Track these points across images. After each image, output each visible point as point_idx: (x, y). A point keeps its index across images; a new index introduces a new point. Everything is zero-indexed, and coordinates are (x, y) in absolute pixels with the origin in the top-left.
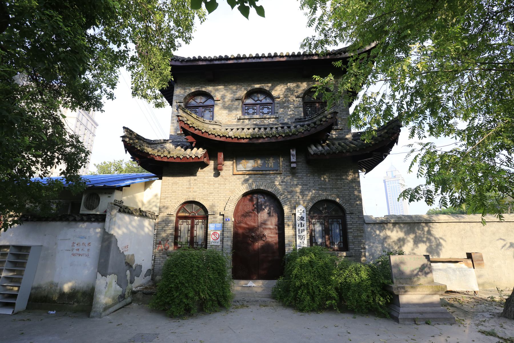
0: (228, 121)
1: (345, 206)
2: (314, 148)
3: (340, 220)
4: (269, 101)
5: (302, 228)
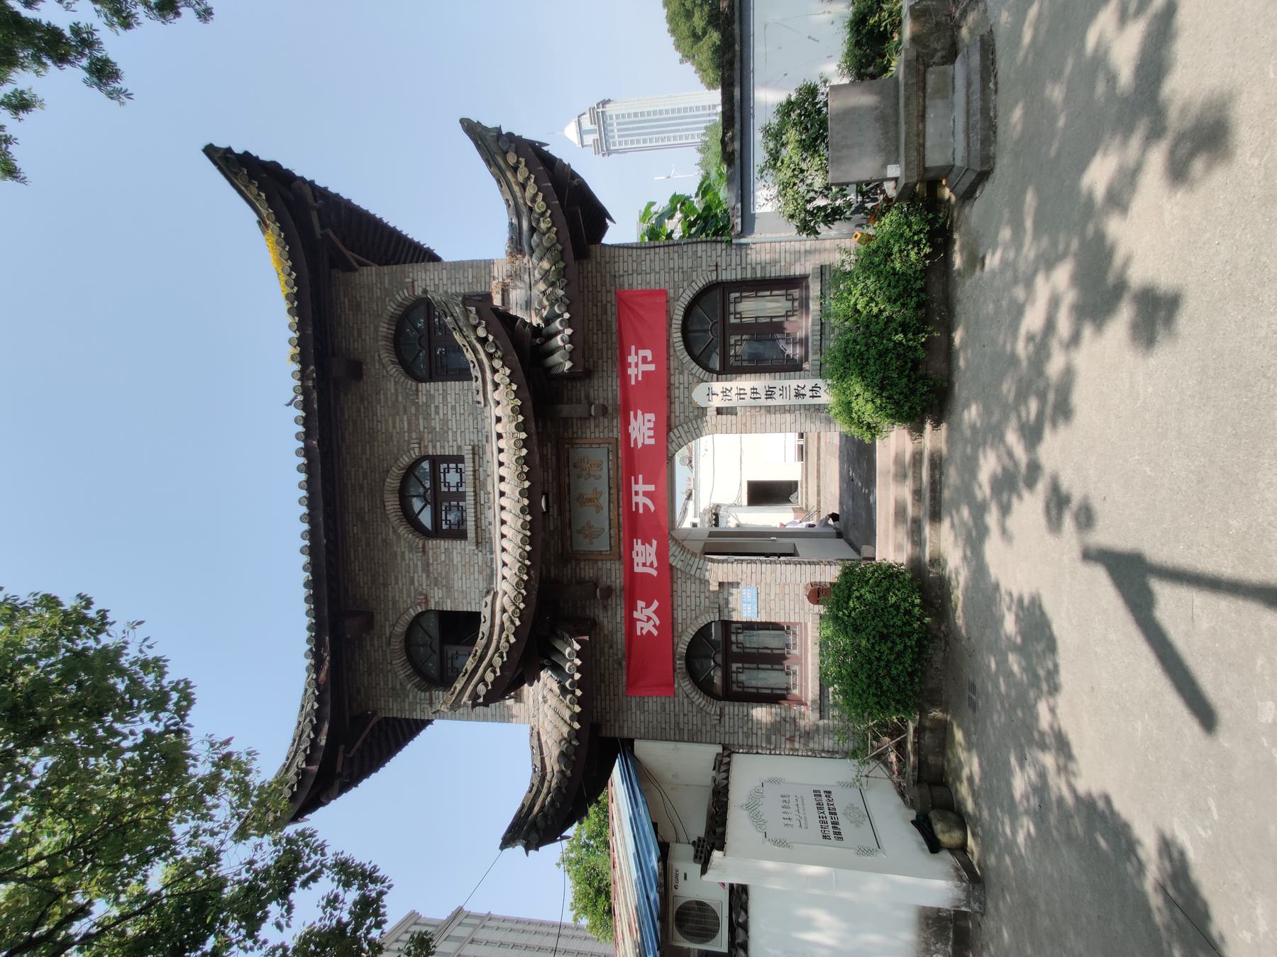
0: (480, 573)
1: (700, 283)
2: (557, 358)
3: (733, 295)
4: (426, 465)
5: (748, 391)
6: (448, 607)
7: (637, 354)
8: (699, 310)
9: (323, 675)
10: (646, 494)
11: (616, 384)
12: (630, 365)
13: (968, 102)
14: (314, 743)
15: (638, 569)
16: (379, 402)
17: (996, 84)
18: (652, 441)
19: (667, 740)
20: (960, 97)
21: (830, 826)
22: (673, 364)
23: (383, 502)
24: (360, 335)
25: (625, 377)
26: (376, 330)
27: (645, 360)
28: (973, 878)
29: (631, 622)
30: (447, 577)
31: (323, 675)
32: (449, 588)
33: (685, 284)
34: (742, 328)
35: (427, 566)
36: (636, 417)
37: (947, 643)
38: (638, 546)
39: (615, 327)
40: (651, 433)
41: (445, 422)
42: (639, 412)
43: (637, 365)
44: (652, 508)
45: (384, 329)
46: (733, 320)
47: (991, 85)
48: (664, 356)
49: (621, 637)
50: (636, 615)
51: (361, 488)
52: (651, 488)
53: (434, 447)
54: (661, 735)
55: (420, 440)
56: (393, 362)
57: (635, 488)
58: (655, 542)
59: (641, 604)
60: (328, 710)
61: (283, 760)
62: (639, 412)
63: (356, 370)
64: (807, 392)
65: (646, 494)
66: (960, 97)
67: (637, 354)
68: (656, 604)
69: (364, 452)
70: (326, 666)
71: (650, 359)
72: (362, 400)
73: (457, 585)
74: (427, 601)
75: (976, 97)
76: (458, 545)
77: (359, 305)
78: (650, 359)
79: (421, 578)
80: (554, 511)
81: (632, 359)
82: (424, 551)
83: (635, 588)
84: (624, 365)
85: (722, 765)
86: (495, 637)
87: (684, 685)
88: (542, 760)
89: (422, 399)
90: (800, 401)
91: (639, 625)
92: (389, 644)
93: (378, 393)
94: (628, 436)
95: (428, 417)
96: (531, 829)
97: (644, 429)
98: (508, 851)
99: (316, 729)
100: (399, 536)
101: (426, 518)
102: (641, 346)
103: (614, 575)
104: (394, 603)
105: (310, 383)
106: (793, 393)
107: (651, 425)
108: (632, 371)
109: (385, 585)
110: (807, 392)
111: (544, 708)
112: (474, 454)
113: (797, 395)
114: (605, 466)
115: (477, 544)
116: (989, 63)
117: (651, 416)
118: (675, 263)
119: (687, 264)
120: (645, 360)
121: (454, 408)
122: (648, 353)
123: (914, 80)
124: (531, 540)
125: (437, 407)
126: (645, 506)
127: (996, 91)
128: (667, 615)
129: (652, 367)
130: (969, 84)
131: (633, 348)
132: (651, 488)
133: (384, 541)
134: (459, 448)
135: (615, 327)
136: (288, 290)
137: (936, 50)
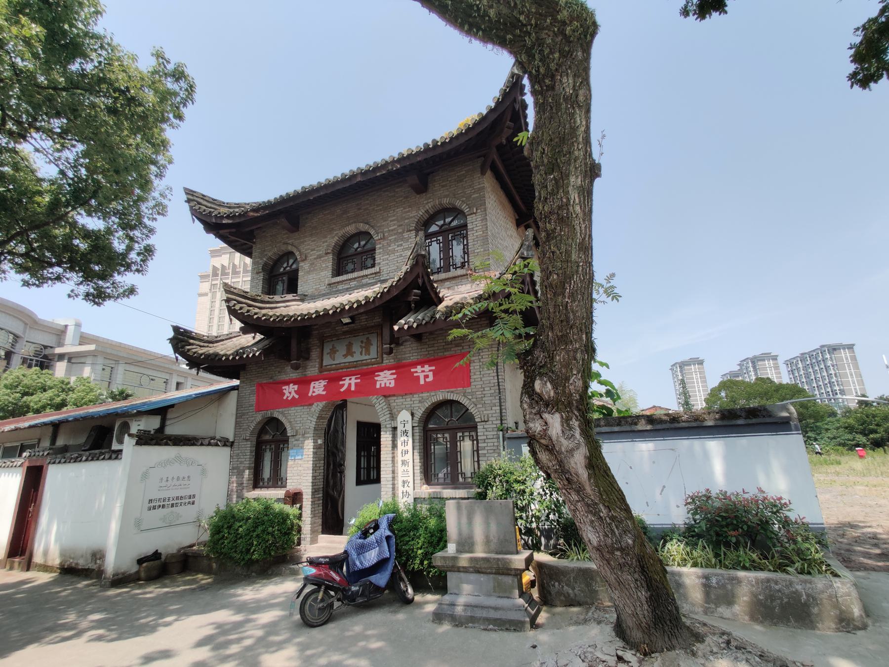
0: (316, 289)
5: (406, 448)
6: (300, 274)
7: (430, 371)
8: (439, 413)
9: (252, 214)
10: (350, 385)
11: (414, 358)
12: (423, 367)
13: (483, 607)
14: (222, 217)
15: (312, 384)
16: (405, 208)
17: (491, 630)
18: (378, 386)
19: (237, 409)
20: (493, 601)
21: (161, 504)
22: (425, 395)
23: (350, 224)
24: (443, 186)
25: (414, 364)
26: (446, 196)
27: (426, 377)
28: (120, 580)
29: (287, 383)
30: (314, 270)
31: (252, 214)
32: (309, 272)
33: (474, 400)
34: (454, 442)
35: (320, 257)
36: (392, 374)
37: (245, 576)
38: (323, 383)
39: (447, 354)
40: (383, 386)
41: (394, 251)
42: (395, 376)
43: (423, 371)
44: (342, 390)
45: (446, 201)
46: (460, 434)
47: (491, 627)
48: (428, 387)
49: (284, 377)
50: (291, 385)
51: (359, 209)
52: (353, 388)
53: (380, 248)
54: (239, 405)
55: (384, 238)
56: (427, 212)
57: (353, 377)
58: (324, 393)
59: (296, 387)
60: (237, 221)
61: (226, 201)
62: (395, 376)
63: (422, 188)
64: (406, 488)
65: (350, 385)
66: (493, 601)
67: (430, 371)
68: (297, 397)
69: (378, 206)
70: (256, 215)
71: (428, 380)
72: (405, 198)
73: (310, 277)
74: (303, 261)
75: (484, 614)
76: (329, 273)
77: (461, 181)
78: (428, 380)
79: (315, 254)
80: (345, 328)
81: (427, 368)
82: (327, 254)
83: (304, 383)
84: (422, 363)
85: (226, 443)
86: (268, 305)
87: (259, 417)
88: (223, 340)
89: (406, 235)
90: (400, 484)
91: (286, 387)
92: (284, 243)
93: (410, 207)
94: (382, 370)
95: (396, 240)
96: (181, 339)
97: (385, 380)
98: (171, 329)
99: (253, 210)
100: (333, 237)
101: (434, 228)
102: (435, 373)
103: (312, 370)
104: (303, 242)
105: (390, 168)
106: (405, 479)
107: (388, 385)
108: (419, 369)
109: (311, 235)
110: (406, 488)
111: (236, 340)
112: (375, 273)
113: (404, 482)
114: (367, 357)
115: (330, 285)
116: (508, 626)
117: (392, 385)
118: (488, 391)
119: (487, 400)
120: (426, 377)
121: (401, 255)
122: (430, 379)
123: (501, 566)
124: (318, 316)
125: (401, 245)
126: (343, 385)
127: (485, 630)
128: (293, 403)
129: (422, 382)
130: (496, 609)
131: (433, 368)
132: (353, 388)
133: (333, 229)
134: (379, 264)
135: (447, 354)
136: (438, 139)
137: (573, 589)
